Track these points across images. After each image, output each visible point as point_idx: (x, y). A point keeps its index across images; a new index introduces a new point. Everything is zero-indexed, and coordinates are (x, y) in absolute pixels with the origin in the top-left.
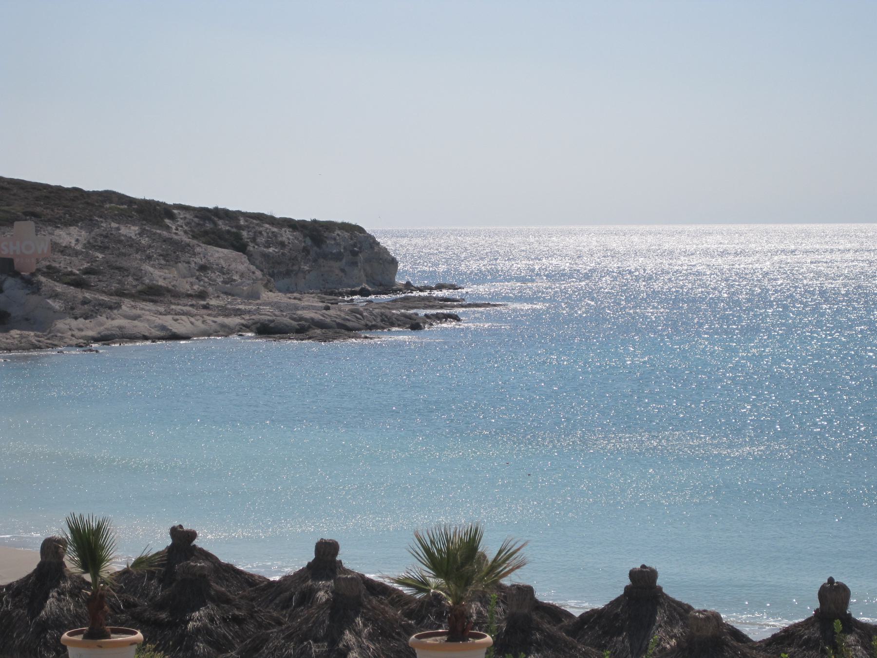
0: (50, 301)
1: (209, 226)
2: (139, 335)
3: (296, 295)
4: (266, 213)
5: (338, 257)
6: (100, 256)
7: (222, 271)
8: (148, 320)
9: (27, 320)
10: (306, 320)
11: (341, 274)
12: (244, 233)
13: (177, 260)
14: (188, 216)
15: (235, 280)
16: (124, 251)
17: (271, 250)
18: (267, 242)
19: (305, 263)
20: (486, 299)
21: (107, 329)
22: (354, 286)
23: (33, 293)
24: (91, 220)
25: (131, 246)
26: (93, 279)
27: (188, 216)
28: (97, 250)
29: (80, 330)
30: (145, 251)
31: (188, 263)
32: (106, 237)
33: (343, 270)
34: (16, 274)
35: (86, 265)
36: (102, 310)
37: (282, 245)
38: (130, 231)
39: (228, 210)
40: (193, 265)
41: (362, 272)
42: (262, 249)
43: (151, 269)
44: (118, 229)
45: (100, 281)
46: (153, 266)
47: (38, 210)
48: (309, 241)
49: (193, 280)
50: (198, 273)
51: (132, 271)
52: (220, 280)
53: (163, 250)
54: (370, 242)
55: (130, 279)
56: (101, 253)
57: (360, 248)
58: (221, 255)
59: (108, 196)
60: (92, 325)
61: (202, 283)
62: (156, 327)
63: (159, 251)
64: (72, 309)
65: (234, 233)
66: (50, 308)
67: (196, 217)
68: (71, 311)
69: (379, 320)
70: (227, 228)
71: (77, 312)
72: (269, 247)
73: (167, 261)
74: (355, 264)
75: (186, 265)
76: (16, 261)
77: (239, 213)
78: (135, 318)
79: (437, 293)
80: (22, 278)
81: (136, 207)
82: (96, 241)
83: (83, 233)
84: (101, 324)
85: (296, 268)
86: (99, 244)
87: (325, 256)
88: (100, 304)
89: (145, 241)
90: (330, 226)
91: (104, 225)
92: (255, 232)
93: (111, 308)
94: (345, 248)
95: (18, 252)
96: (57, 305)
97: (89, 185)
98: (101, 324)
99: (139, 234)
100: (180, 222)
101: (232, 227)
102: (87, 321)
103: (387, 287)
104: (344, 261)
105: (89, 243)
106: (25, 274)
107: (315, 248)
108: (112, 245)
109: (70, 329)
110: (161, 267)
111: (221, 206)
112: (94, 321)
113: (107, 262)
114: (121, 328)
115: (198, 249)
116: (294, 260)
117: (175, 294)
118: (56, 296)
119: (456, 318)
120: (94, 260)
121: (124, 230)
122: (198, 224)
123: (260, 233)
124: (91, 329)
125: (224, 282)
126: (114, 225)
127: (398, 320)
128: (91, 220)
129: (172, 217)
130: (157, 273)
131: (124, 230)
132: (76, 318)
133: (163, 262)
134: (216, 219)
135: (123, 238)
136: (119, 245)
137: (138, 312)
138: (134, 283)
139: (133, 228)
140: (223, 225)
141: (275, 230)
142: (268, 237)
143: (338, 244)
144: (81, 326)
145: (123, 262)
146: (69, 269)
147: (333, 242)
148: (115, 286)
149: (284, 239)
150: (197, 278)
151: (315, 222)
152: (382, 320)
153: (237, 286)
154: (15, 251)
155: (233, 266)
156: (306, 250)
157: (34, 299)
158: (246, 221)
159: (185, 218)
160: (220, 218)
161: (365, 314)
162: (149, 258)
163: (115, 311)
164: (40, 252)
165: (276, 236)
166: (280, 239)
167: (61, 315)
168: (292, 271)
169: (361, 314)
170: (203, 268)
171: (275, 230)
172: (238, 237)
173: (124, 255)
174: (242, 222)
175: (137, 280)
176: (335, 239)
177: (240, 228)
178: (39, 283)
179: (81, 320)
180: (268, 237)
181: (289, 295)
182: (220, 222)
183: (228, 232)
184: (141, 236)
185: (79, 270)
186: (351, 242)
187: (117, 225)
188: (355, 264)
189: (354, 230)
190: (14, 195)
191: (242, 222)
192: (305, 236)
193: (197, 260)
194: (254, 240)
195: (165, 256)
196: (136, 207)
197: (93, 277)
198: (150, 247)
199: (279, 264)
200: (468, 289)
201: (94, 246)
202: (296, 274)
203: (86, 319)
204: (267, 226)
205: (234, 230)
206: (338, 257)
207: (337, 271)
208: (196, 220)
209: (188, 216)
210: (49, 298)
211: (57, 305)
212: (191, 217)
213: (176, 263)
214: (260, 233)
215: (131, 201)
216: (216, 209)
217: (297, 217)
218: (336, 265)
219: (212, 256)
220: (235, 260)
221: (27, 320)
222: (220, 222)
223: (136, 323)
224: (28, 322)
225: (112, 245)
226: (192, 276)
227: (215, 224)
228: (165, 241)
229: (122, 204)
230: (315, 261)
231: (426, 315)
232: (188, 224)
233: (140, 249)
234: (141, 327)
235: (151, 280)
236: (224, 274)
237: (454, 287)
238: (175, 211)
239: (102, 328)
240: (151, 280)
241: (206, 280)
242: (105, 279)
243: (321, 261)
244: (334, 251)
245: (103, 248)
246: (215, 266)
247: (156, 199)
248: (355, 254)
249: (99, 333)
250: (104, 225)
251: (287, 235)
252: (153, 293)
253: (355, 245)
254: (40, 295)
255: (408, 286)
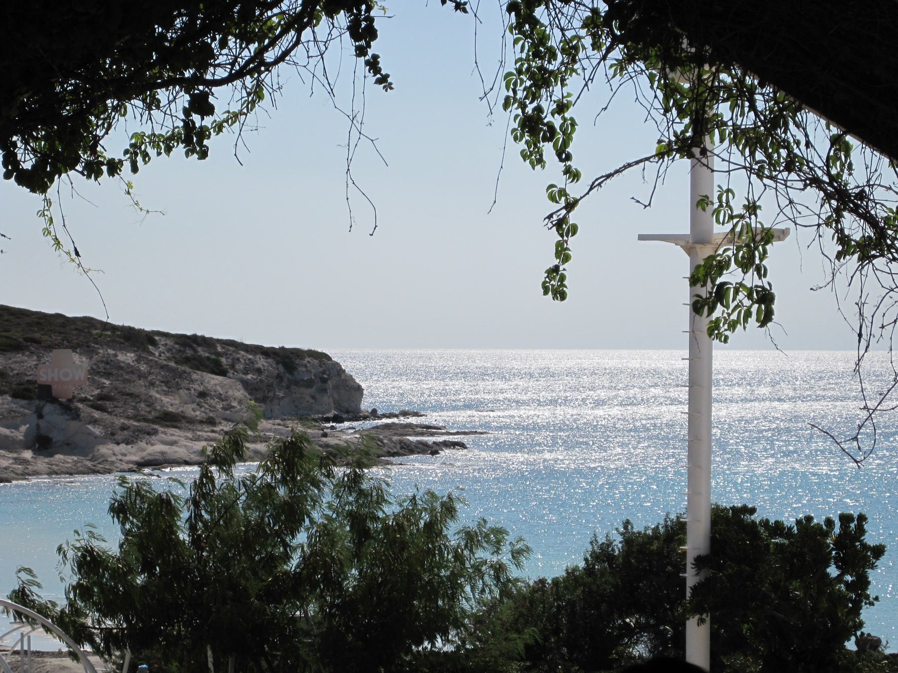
0: (90, 427)
1: (189, 352)
2: (180, 460)
3: (278, 421)
4: (236, 340)
5: (309, 384)
6: (107, 382)
7: (220, 397)
8: (186, 446)
9: (68, 444)
10: (332, 446)
11: (312, 401)
12: (223, 360)
13: (178, 387)
14: (168, 342)
15: (234, 407)
16: (127, 377)
17: (249, 377)
18: (245, 368)
19: (280, 390)
20: (467, 428)
21: (150, 454)
22: (324, 413)
23: (74, 419)
24: (88, 346)
25: (132, 372)
26: (108, 404)
27: (168, 342)
28: (102, 376)
29: (125, 455)
30: (146, 378)
31: (188, 389)
32: (107, 363)
33: (313, 397)
34: (54, 400)
35: (97, 392)
36: (141, 435)
37: (259, 371)
38: (127, 357)
39: (133, 329)
40: (193, 391)
41: (331, 400)
42: (241, 375)
43: (158, 396)
44: (116, 355)
45: (116, 407)
46: (158, 392)
47: (37, 335)
48: (281, 369)
49: (194, 406)
50: (198, 400)
51: (143, 397)
52: (219, 406)
53: (163, 377)
54: (337, 370)
55: (143, 405)
56: (108, 379)
57: (329, 375)
58: (217, 382)
59: (89, 322)
60: (133, 450)
61: (203, 409)
62: (194, 452)
63: (159, 377)
64: (113, 434)
65: (213, 360)
66: (90, 434)
67: (177, 343)
68: (112, 436)
69: (398, 446)
70: (207, 355)
71: (118, 437)
72: (247, 374)
73: (169, 388)
74: (324, 391)
75: (187, 392)
76: (54, 387)
77: (219, 341)
78: (173, 443)
79: (403, 420)
80: (61, 404)
81: (119, 333)
82: (98, 367)
83: (84, 359)
84: (143, 450)
85: (271, 394)
86: (102, 370)
87: (297, 383)
88: (139, 431)
89: (143, 368)
90: (297, 353)
91: (101, 351)
92: (233, 359)
93: (149, 434)
94: (315, 375)
95: (56, 379)
96: (97, 431)
97: (72, 312)
98: (143, 450)
99: (136, 360)
100: (162, 349)
101: (211, 354)
102: (129, 447)
103: (356, 415)
104: (314, 388)
105: (92, 369)
106: (63, 400)
107: (287, 375)
108: (114, 371)
109: (114, 454)
110: (166, 394)
111: (199, 334)
112: (135, 447)
113: (116, 389)
114: (163, 453)
115: (194, 376)
116: (270, 386)
117: (191, 421)
118: (95, 422)
119: (462, 446)
120: (101, 386)
121: (121, 357)
122: (180, 351)
123: (238, 359)
124: (134, 454)
125: (224, 408)
126: (111, 352)
127: (417, 447)
128: (88, 346)
129: (154, 343)
130: (166, 400)
131: (121, 357)
132: (118, 444)
133: (165, 388)
134: (195, 346)
135: (122, 364)
136: (121, 372)
137: (174, 438)
138: (148, 409)
139: (128, 354)
140: (202, 352)
141: (250, 357)
142: (246, 364)
143: (309, 372)
144: (124, 451)
145: (133, 390)
146: (83, 396)
147: (304, 369)
148: (130, 412)
149: (259, 365)
150: (198, 405)
151: (283, 348)
152: (402, 448)
153: (237, 412)
154: (53, 378)
155: (230, 393)
156: (279, 377)
157: (74, 424)
158: (223, 348)
159: (166, 345)
160: (199, 345)
161: (385, 441)
162: (152, 384)
163: (153, 437)
164: (77, 379)
165: (253, 363)
166: (256, 366)
167: (103, 440)
168: (268, 397)
169: (382, 442)
170: (203, 395)
171: (250, 357)
172: (218, 363)
173: (129, 381)
174: (219, 349)
175: (149, 406)
176: (306, 366)
177: (219, 354)
178: (78, 409)
179: (123, 446)
180: (246, 364)
181: (271, 421)
182: (199, 349)
183: (208, 358)
184: (139, 363)
185: (92, 396)
186: (321, 369)
187: (113, 352)
188: (324, 391)
189: (322, 357)
190: (7, 321)
191: (219, 349)
192: (277, 363)
193: (196, 386)
194: (233, 366)
195: (166, 383)
196: (119, 333)
197: (108, 403)
198: (150, 373)
199: (256, 390)
200: (432, 418)
201: (99, 373)
202: (272, 400)
203: (127, 444)
204: (243, 353)
205: (213, 357)
206: (309, 384)
207: (308, 398)
208: (177, 346)
209: (170, 342)
210: (89, 423)
211: (97, 431)
212: (172, 344)
213: (178, 389)
214: (238, 359)
215: (114, 328)
216: (195, 336)
217: (266, 345)
218: (307, 392)
219: (208, 382)
220: (231, 387)
221: (68, 444)
222: (199, 349)
223: (174, 448)
224: (69, 447)
225: (114, 371)
226: (193, 402)
227: (195, 351)
228: (162, 368)
229: (106, 330)
230: (288, 387)
231: (434, 443)
232: (169, 350)
233: (142, 376)
234: (180, 452)
235: (162, 407)
236: (223, 400)
237: (416, 414)
238: (157, 338)
239: (145, 453)
240: (162, 407)
241: (206, 406)
242: (120, 405)
243: (293, 387)
244: (306, 378)
245: (108, 375)
246: (213, 393)
247: (137, 326)
248: (324, 381)
249: (143, 458)
250: (101, 351)
251: (261, 362)
252: (171, 419)
253: (324, 372)
254: (80, 421)
255: (374, 414)
